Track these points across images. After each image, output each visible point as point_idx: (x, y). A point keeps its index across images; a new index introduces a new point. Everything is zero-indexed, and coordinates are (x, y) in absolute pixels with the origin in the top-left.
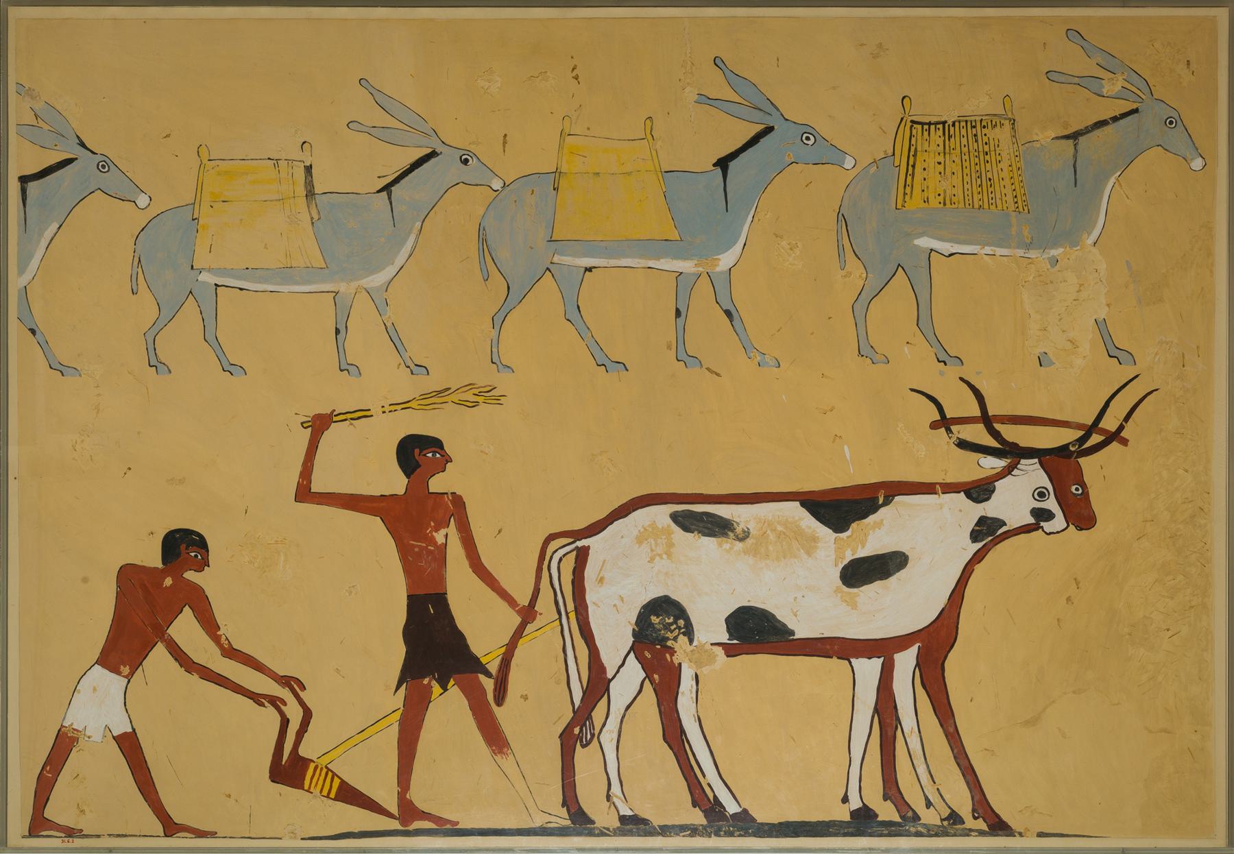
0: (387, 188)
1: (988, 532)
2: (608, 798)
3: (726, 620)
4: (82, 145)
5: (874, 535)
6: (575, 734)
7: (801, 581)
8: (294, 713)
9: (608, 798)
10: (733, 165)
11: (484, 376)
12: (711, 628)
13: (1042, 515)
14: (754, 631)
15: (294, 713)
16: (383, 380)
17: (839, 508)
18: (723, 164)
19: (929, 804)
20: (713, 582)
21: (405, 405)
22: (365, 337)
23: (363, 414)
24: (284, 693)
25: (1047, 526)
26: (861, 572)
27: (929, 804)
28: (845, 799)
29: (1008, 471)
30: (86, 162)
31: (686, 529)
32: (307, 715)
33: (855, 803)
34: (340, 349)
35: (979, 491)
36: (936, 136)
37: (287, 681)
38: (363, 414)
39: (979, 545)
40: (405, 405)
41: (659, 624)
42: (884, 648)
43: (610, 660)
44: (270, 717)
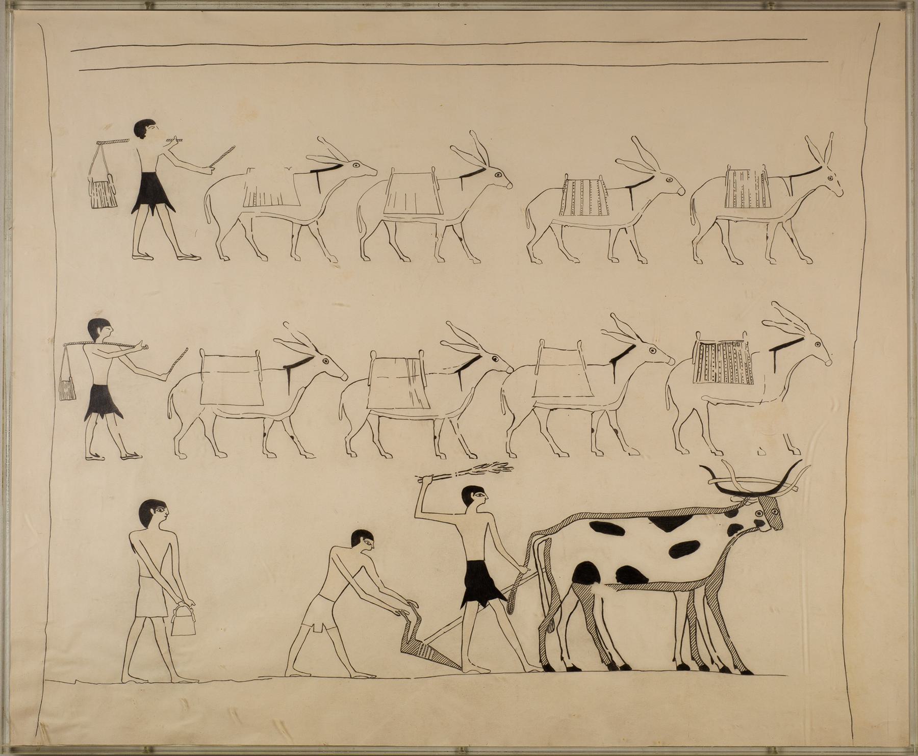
0: (459, 371)
1: (734, 529)
2: (562, 659)
3: (617, 573)
4: (317, 350)
5: (681, 535)
6: (548, 626)
7: (645, 547)
8: (412, 617)
9: (562, 659)
10: (618, 362)
11: (503, 458)
12: (608, 573)
13: (759, 524)
14: (629, 577)
15: (412, 617)
16: (457, 461)
17: (668, 522)
18: (614, 361)
19: (713, 662)
20: (609, 555)
21: (467, 472)
22: (448, 441)
23: (448, 476)
24: (409, 609)
25: (762, 528)
26: (681, 550)
27: (713, 662)
28: (674, 660)
29: (743, 504)
30: (318, 359)
31: (597, 530)
32: (419, 619)
33: (679, 663)
34: (436, 446)
35: (732, 513)
36: (711, 350)
37: (410, 603)
38: (448, 476)
39: (731, 538)
40: (467, 472)
41: (586, 574)
42: (690, 587)
43: (562, 591)
44: (402, 621)
